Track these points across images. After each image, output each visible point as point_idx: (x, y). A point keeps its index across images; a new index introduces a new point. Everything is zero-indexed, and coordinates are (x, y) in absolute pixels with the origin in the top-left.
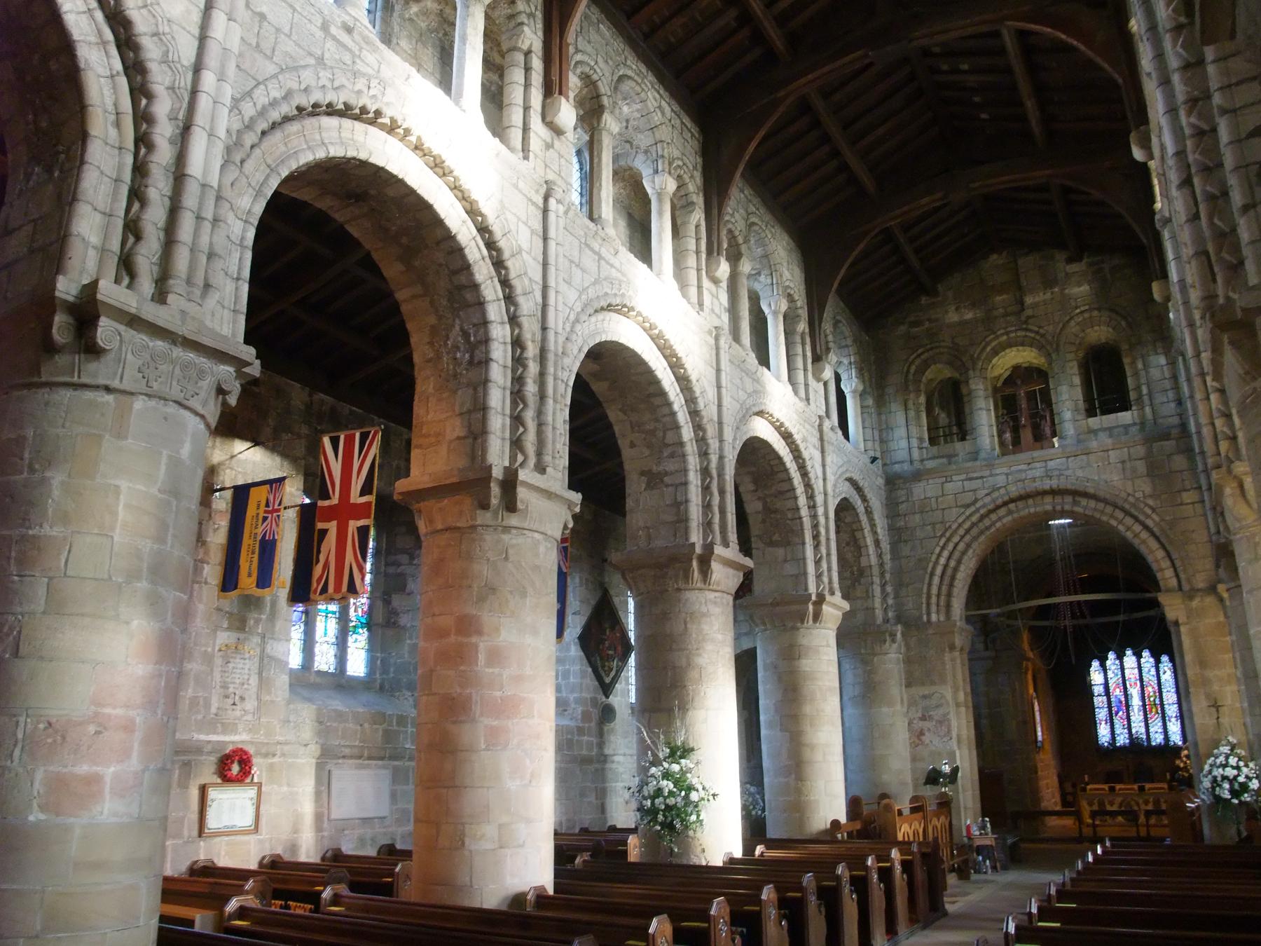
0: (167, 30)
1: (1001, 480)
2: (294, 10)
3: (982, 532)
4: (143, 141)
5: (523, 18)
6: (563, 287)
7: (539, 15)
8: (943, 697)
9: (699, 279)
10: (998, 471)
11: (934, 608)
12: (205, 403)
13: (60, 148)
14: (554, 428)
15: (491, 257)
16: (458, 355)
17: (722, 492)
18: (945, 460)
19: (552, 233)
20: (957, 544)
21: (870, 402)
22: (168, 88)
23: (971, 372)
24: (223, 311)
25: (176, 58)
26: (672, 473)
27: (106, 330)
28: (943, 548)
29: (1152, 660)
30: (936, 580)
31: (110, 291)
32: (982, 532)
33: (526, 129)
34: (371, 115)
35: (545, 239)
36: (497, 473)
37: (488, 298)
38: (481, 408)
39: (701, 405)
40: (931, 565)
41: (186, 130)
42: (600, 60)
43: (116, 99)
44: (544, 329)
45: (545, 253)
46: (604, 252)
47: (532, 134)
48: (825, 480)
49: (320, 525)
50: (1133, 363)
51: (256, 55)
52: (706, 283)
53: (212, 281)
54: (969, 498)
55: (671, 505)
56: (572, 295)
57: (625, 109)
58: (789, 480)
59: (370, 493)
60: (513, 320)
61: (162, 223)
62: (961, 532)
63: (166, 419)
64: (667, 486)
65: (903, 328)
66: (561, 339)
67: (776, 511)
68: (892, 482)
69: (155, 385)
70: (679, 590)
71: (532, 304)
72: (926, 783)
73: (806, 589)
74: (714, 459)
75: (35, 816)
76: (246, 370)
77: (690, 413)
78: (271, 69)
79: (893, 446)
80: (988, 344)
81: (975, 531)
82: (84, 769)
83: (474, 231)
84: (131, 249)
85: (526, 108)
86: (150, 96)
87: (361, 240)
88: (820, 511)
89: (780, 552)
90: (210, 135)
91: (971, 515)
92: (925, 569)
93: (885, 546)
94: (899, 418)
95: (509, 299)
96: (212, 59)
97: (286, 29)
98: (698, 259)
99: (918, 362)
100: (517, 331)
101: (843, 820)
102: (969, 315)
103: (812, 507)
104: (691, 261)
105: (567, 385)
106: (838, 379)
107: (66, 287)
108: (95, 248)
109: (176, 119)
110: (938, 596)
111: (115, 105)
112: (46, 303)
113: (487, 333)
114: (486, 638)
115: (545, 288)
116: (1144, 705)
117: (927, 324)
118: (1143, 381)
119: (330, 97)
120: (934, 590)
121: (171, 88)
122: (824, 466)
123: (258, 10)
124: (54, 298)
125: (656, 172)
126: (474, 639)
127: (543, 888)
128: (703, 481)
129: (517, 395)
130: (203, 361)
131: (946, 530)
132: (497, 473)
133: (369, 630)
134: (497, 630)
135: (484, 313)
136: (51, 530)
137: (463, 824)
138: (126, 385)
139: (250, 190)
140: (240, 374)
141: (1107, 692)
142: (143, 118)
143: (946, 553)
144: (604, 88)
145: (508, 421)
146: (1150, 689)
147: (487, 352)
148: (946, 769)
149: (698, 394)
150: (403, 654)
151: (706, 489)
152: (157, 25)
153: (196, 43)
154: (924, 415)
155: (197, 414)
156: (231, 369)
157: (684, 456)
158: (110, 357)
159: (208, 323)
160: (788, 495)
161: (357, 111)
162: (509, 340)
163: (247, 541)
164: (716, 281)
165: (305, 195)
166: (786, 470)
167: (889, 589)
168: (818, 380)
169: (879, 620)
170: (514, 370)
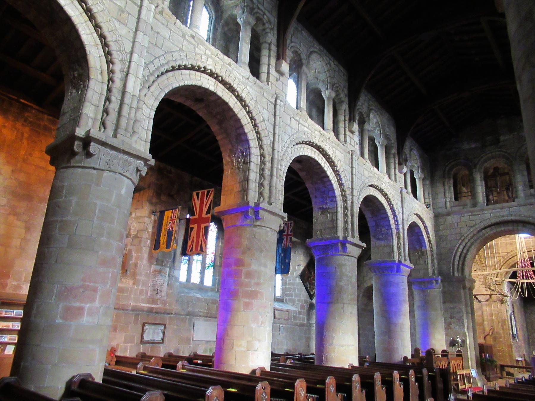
0: (120, 39)
1: (487, 216)
2: (171, 30)
5: (268, 30)
6: (281, 134)
7: (276, 29)
8: (460, 309)
9: (345, 131)
11: (456, 270)
12: (132, 174)
14: (276, 188)
17: (352, 216)
18: (461, 207)
21: (428, 182)
23: (474, 170)
24: (141, 141)
26: (331, 208)
27: (93, 147)
28: (460, 244)
30: (457, 258)
32: (478, 238)
35: (275, 115)
36: (252, 204)
38: (246, 180)
39: (343, 182)
40: (454, 251)
42: (302, 45)
44: (273, 150)
46: (301, 121)
47: (270, 75)
48: (403, 213)
49: (191, 226)
51: (156, 48)
52: (348, 133)
53: (136, 130)
54: (472, 223)
55: (331, 221)
56: (286, 138)
57: (314, 65)
58: (386, 213)
59: (209, 213)
60: (261, 147)
61: (117, 109)
62: (469, 238)
66: (280, 154)
69: (112, 167)
70: (333, 255)
71: (269, 141)
73: (394, 258)
75: (59, 321)
76: (148, 163)
78: (161, 53)
81: (475, 238)
82: (77, 304)
85: (269, 65)
87: (203, 117)
89: (382, 243)
91: (473, 231)
95: (259, 139)
98: (345, 124)
99: (449, 166)
100: (262, 151)
101: (410, 357)
102: (473, 146)
105: (284, 172)
106: (412, 173)
107: (80, 132)
108: (91, 118)
109: (123, 71)
110: (458, 265)
111: (101, 67)
112: (73, 138)
119: (185, 62)
120: (456, 262)
121: (122, 60)
122: (402, 208)
125: (327, 89)
126: (241, 268)
127: (264, 368)
128: (344, 212)
129: (262, 175)
130: (131, 159)
131: (462, 237)
132: (252, 204)
133: (214, 268)
134: (250, 265)
136: (70, 218)
137: (233, 340)
138: (101, 167)
140: (146, 164)
143: (461, 247)
144: (303, 56)
148: (459, 340)
151: (346, 215)
153: (131, 44)
154: (452, 188)
155: (128, 178)
156: (142, 162)
159: (134, 145)
161: (197, 68)
162: (259, 154)
163: (163, 231)
164: (352, 132)
165: (179, 100)
166: (385, 209)
168: (401, 173)
169: (430, 274)
170: (261, 166)
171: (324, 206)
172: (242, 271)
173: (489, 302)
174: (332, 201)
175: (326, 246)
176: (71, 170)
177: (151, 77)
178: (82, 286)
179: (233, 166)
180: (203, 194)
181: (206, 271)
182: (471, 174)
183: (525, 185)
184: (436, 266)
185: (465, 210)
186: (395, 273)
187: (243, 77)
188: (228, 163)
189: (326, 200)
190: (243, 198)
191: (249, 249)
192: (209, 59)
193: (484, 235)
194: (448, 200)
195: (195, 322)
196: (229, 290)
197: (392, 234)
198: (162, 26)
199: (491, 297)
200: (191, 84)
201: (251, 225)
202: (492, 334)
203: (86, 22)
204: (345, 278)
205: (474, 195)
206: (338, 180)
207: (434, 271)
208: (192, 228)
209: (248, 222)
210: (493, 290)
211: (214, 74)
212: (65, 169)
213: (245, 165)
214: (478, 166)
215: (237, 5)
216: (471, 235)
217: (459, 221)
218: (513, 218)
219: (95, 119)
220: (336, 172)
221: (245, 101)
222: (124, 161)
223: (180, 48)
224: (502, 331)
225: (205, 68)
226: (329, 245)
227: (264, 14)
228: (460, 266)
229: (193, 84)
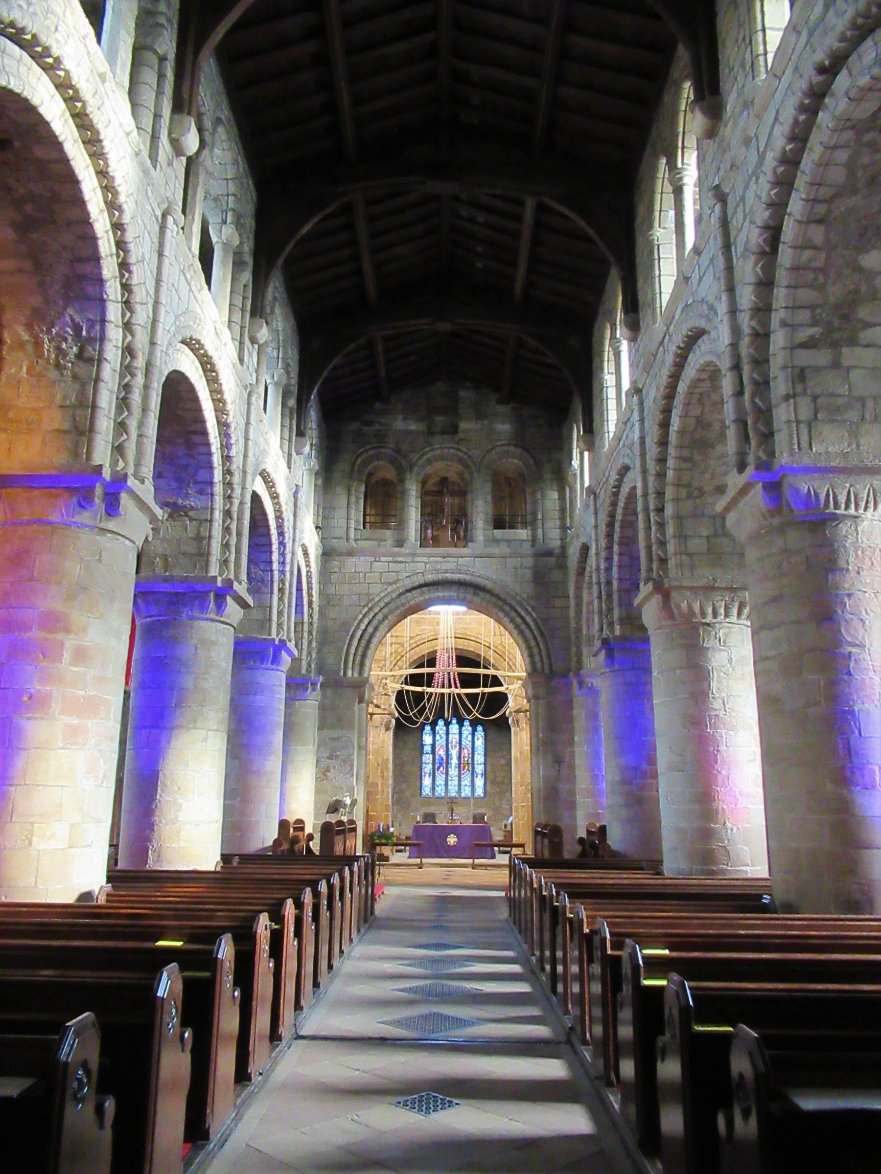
1: (420, 567)
3: (397, 607)
9: (242, 335)
10: (419, 559)
16: (64, 346)
18: (375, 543)
20: (376, 614)
23: (408, 475)
28: (364, 616)
29: (470, 728)
30: (356, 641)
32: (397, 607)
48: (294, 540)
50: (534, 492)
54: (393, 577)
60: (128, 327)
62: (382, 604)
65: (355, 425)
70: (192, 618)
72: (327, 813)
74: (236, 502)
79: (334, 523)
80: (425, 453)
83: (109, 226)
91: (392, 591)
94: (343, 500)
99: (364, 456)
100: (129, 338)
102: (413, 427)
110: (355, 655)
114: (72, 636)
115: (156, 303)
116: (459, 764)
117: (377, 427)
118: (540, 508)
120: (353, 651)
125: (224, 222)
126: (60, 636)
131: (369, 601)
134: (85, 630)
141: (433, 752)
143: (366, 621)
146: (466, 751)
148: (348, 801)
151: (227, 530)
157: (212, 495)
160: (265, 549)
162: (120, 345)
166: (268, 527)
167: (314, 644)
170: (122, 377)
171: (180, 501)
172: (62, 645)
174: (201, 492)
175: (177, 594)
179: (41, 356)
182: (402, 481)
183: (486, 521)
184: (314, 655)
186: (269, 665)
188: (21, 345)
189: (188, 486)
190: (76, 454)
191: (85, 589)
193: (408, 602)
194: (353, 524)
197: (272, 581)
200: (18, 91)
201: (92, 527)
204: (214, 672)
206: (222, 445)
207: (309, 665)
209: (85, 517)
210: (377, 706)
211: (72, 87)
213: (82, 364)
214: (416, 469)
218: (461, 576)
221: (116, 194)
224: (380, 782)
225: (58, 60)
228: (358, 658)
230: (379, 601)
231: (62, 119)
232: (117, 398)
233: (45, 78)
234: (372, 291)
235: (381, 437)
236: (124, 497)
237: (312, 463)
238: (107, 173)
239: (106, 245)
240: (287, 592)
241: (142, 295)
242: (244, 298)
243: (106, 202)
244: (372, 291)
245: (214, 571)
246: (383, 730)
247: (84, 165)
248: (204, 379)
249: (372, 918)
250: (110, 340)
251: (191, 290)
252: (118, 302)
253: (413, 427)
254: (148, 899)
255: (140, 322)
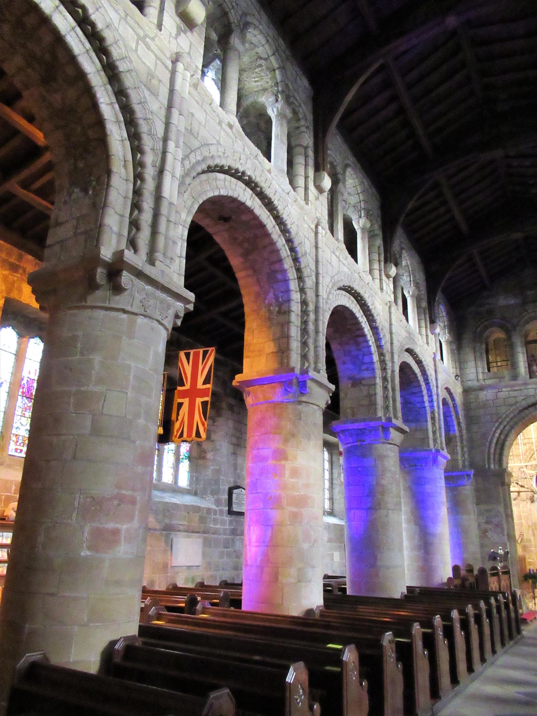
0: (151, 117)
2: (207, 113)
4: (138, 177)
5: (303, 129)
7: (311, 128)
9: (380, 275)
10: (530, 387)
11: (492, 460)
13: (92, 178)
15: (292, 256)
18: (497, 380)
19: (320, 245)
20: (505, 427)
22: (151, 149)
25: (155, 133)
27: (126, 278)
28: (497, 428)
30: (493, 445)
31: (129, 255)
33: (306, 188)
34: (240, 174)
37: (291, 278)
41: (161, 172)
43: (125, 152)
45: (317, 256)
48: (437, 387)
52: (384, 278)
54: (512, 401)
55: (366, 396)
60: (302, 290)
62: (508, 419)
63: (153, 329)
64: (364, 385)
67: (410, 403)
68: (466, 391)
69: (148, 311)
71: (311, 282)
73: (429, 447)
74: (389, 372)
75: (85, 553)
77: (377, 347)
79: (467, 371)
82: (111, 525)
83: (284, 242)
84: (134, 235)
85: (306, 177)
86: (142, 152)
88: (435, 404)
90: (172, 176)
92: (487, 439)
93: (463, 425)
96: (173, 135)
97: (203, 123)
102: (512, 302)
103: (431, 401)
104: (376, 266)
108: (116, 233)
110: (494, 454)
112: (95, 259)
113: (289, 296)
114: (289, 462)
117: (487, 307)
120: (492, 450)
123: (191, 111)
124: (99, 258)
125: (360, 217)
126: (283, 462)
129: (304, 331)
134: (295, 458)
135: (288, 286)
138: (134, 310)
139: (186, 210)
142: (138, 165)
143: (499, 431)
145: (299, 344)
147: (289, 307)
148: (501, 552)
149: (381, 336)
150: (209, 473)
151: (385, 388)
152: (146, 114)
153: (164, 126)
157: (374, 369)
158: (126, 293)
162: (299, 301)
167: (465, 449)
170: (302, 317)
172: (284, 466)
173: (517, 501)
176: (88, 313)
177: (186, 179)
178: (114, 498)
180: (196, 355)
181: (181, 465)
182: (509, 338)
184: (466, 456)
185: (503, 384)
187: (283, 190)
191: (293, 435)
192: (249, 161)
195: (174, 540)
196: (266, 495)
198: (197, 105)
199: (519, 495)
202: (521, 542)
203: (105, 85)
204: (388, 475)
205: (514, 366)
207: (464, 462)
208: (180, 405)
210: (522, 486)
211: (253, 182)
212: (76, 311)
215: (265, 90)
216: (512, 415)
217: (495, 398)
219: (120, 235)
220: (375, 329)
221: (285, 225)
222: (162, 302)
223: (217, 141)
224: (532, 538)
226: (365, 429)
227: (300, 105)
228: (497, 456)
229: (229, 194)
230: (505, 418)
231: (252, 199)
232: (301, 329)
233: (240, 183)
234: (464, 227)
235: (490, 312)
236: (309, 383)
237: (447, 337)
238: (279, 216)
239: (285, 252)
240: (437, 419)
241: (308, 271)
242: (379, 254)
243: (281, 231)
244: (464, 227)
245: (380, 413)
246: (529, 502)
247: (266, 216)
248: (358, 306)
249: (519, 637)
250: (293, 300)
251: (340, 261)
252: (295, 279)
253: (512, 302)
254: (416, 611)
255: (308, 287)
